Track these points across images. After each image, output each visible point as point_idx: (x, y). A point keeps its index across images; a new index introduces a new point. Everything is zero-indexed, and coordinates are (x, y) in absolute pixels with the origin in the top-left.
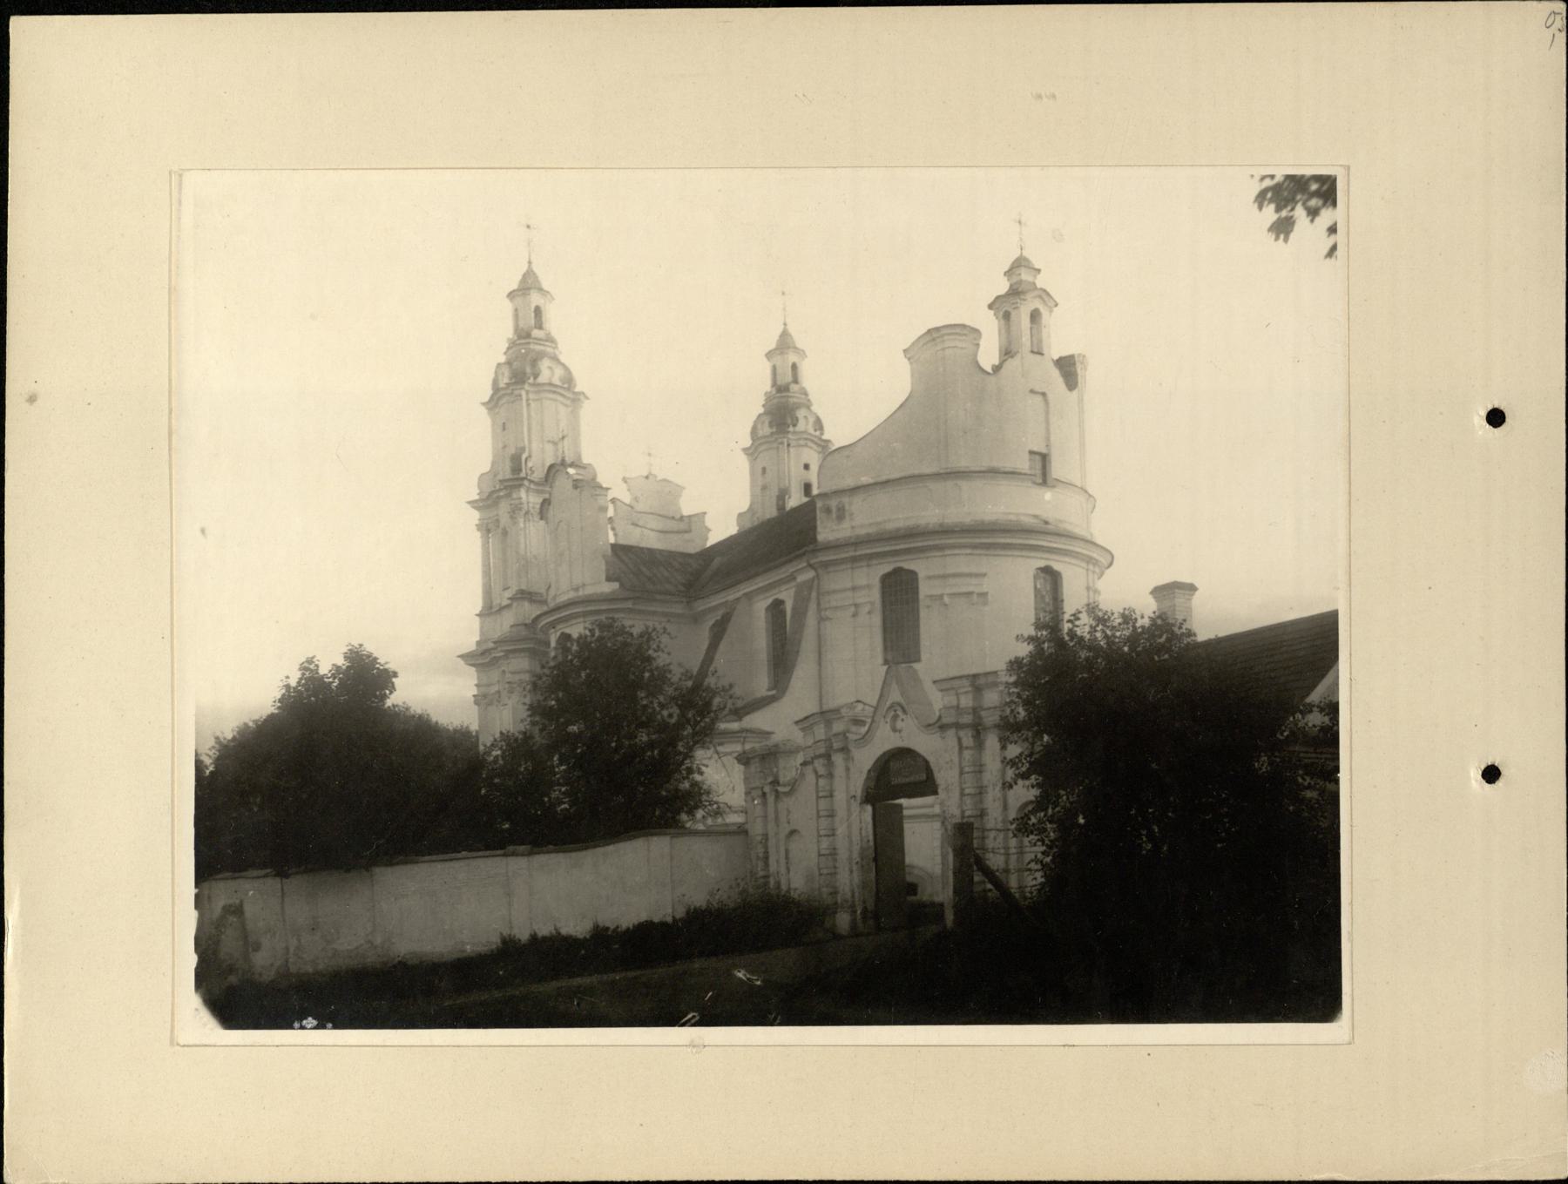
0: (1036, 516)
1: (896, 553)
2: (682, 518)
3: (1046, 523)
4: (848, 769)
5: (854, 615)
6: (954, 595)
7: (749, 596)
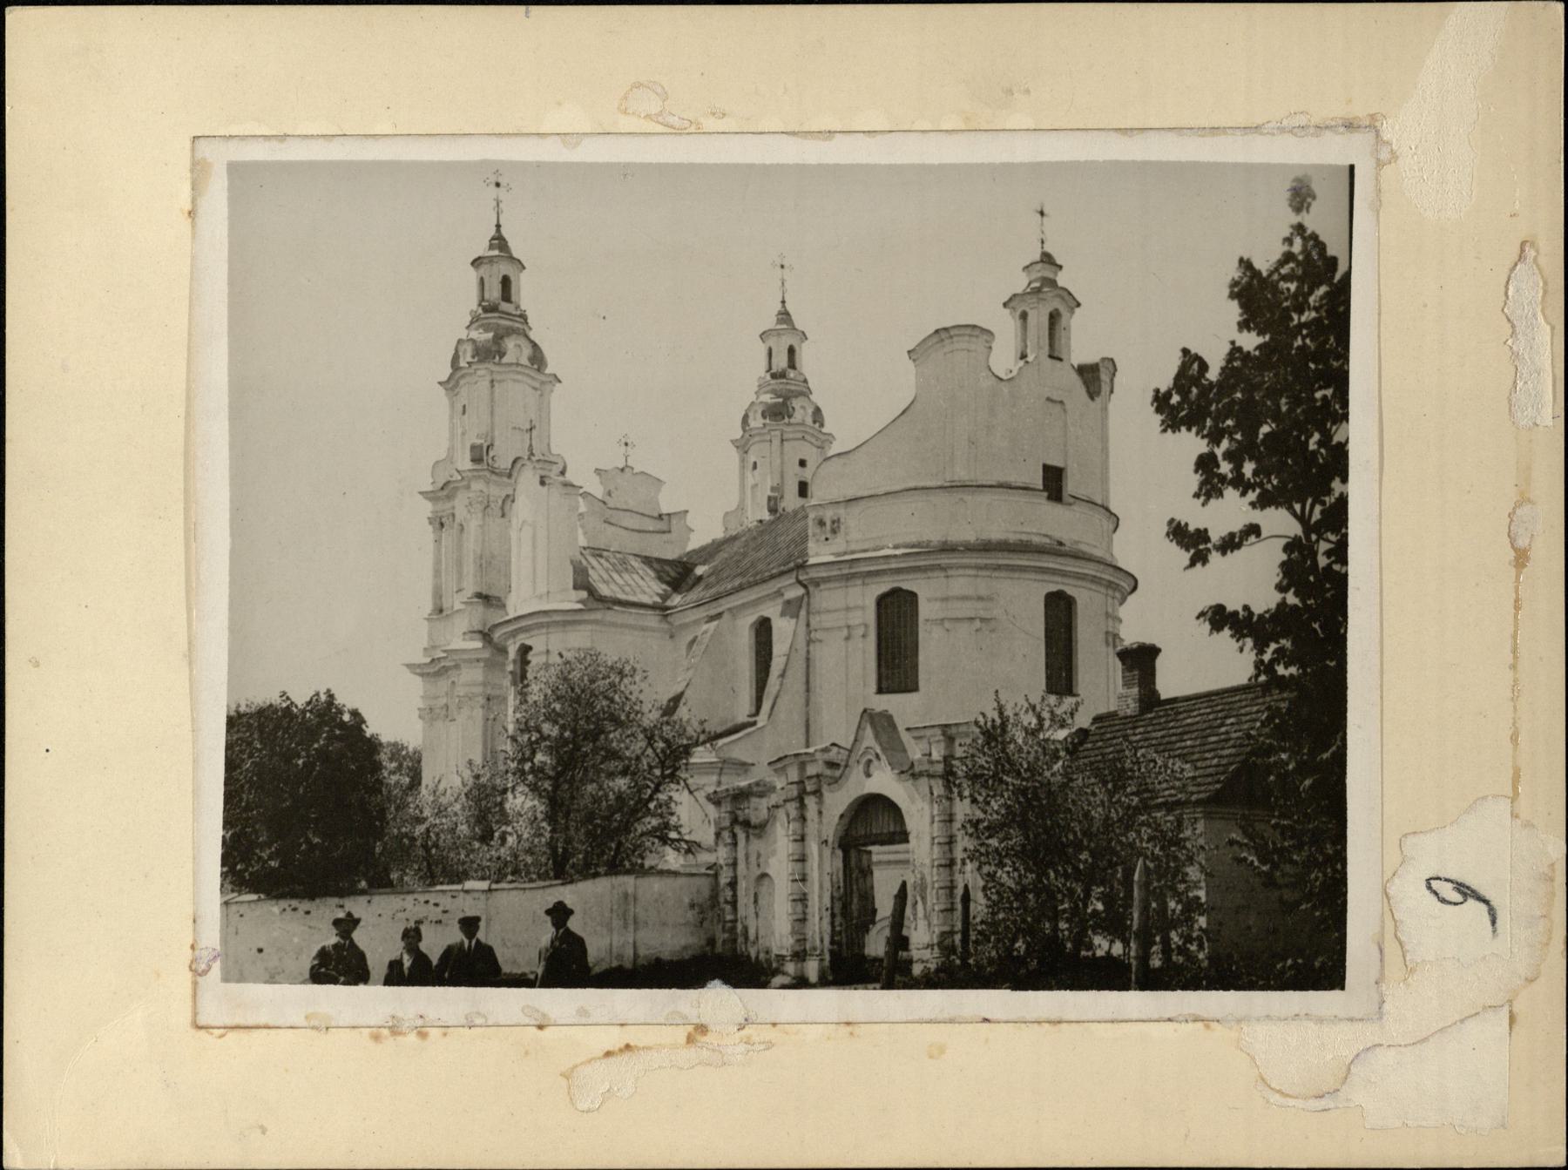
2: (660, 517)
3: (1061, 544)
4: (820, 813)
5: (847, 638)
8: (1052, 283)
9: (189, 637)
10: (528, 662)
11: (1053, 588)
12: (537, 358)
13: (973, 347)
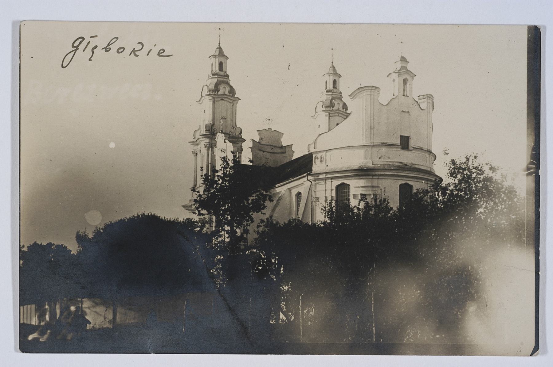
0: (401, 163)
2: (282, 147)
3: (406, 165)
8: (406, 68)
9: (538, 167)
11: (403, 182)
12: (232, 91)
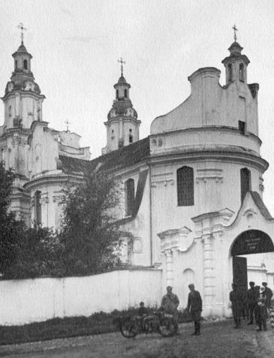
1: (248, 162)
2: (80, 149)
6: (209, 178)
7: (120, 177)
10: (40, 198)
11: (243, 167)
13: (213, 76)
